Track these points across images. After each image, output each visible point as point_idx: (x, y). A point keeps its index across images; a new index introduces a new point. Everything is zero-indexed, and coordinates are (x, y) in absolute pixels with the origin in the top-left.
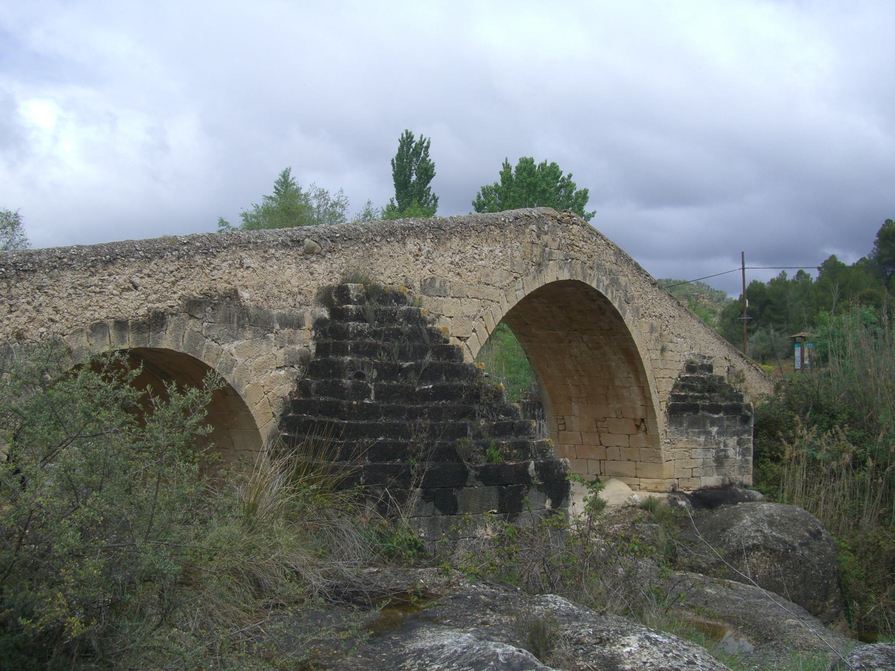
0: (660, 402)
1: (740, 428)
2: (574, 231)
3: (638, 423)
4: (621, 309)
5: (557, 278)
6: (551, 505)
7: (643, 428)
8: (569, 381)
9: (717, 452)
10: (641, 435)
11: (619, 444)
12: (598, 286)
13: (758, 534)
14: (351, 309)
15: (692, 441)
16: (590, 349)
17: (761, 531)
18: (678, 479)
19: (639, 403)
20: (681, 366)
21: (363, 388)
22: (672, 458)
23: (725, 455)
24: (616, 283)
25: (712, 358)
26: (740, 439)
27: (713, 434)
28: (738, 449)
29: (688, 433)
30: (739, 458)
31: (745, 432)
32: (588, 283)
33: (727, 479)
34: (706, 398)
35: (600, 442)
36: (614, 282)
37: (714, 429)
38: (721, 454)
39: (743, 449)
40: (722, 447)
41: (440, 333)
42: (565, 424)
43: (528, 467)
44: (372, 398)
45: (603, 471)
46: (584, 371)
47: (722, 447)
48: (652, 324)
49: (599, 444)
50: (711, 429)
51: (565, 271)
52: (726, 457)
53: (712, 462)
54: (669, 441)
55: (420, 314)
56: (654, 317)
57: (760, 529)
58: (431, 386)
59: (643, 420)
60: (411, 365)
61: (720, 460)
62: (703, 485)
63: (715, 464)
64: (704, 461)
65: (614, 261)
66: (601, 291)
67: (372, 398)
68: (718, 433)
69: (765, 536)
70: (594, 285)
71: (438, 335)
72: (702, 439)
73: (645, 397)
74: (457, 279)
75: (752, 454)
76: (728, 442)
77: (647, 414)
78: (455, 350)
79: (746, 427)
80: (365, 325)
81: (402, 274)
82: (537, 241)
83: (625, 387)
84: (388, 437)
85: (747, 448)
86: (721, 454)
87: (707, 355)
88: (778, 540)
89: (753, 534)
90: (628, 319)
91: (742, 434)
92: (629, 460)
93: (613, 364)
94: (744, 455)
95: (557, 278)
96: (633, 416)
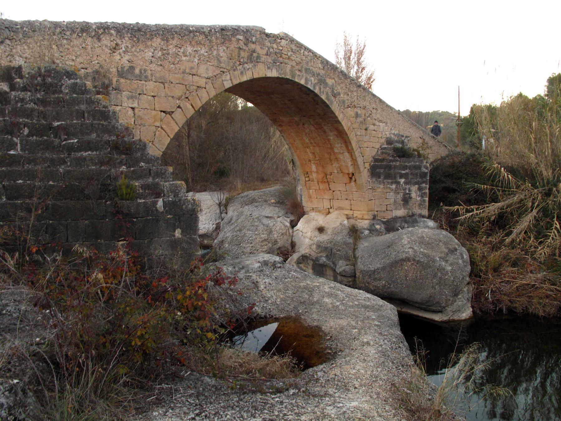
0: (364, 163)
1: (420, 180)
2: (282, 44)
3: (350, 176)
4: (328, 100)
5: (266, 75)
6: (181, 234)
7: (353, 179)
8: (308, 150)
9: (404, 195)
10: (353, 184)
11: (341, 189)
12: (306, 83)
13: (410, 250)
14: (19, 82)
15: (387, 188)
16: (317, 129)
17: (413, 248)
18: (377, 211)
19: (350, 163)
20: (383, 140)
21: (8, 142)
22: (373, 198)
23: (409, 197)
24: (324, 83)
25: (409, 137)
26: (420, 187)
27: (402, 183)
28: (418, 193)
29: (384, 183)
30: (419, 199)
31: (423, 182)
32: (296, 80)
33: (411, 212)
34: (397, 161)
35: (330, 188)
36: (322, 82)
37: (402, 181)
38: (406, 196)
39: (422, 193)
40: (407, 192)
41: (100, 100)
42: (309, 177)
43: (157, 204)
44: (19, 150)
45: (332, 206)
46: (315, 143)
47: (407, 192)
48: (357, 113)
49: (329, 189)
50: (400, 180)
51: (273, 70)
52: (411, 198)
53: (400, 201)
54: (371, 187)
55: (86, 87)
56: (359, 108)
57: (412, 247)
58: (76, 141)
59: (353, 174)
60: (62, 124)
61: (406, 200)
62: (394, 215)
63: (402, 203)
64: (395, 200)
65: (322, 68)
66: (309, 87)
67: (19, 150)
68: (405, 183)
69: (415, 251)
70: (302, 82)
71: (97, 102)
72: (394, 186)
73: (353, 159)
74: (159, 69)
75: (428, 196)
76: (412, 188)
77: (355, 171)
78: (111, 113)
79: (425, 180)
80: (27, 94)
81: (97, 62)
82: (244, 47)
83: (340, 153)
84: (27, 180)
85: (424, 192)
86: (406, 196)
87: (405, 135)
88: (425, 255)
89: (407, 250)
90: (335, 107)
91: (421, 184)
92: (347, 199)
93: (332, 138)
94: (422, 197)
95: (266, 75)
96: (347, 172)
